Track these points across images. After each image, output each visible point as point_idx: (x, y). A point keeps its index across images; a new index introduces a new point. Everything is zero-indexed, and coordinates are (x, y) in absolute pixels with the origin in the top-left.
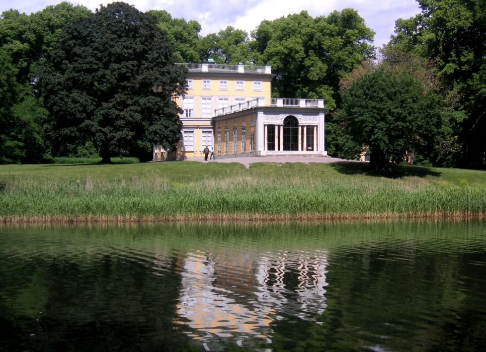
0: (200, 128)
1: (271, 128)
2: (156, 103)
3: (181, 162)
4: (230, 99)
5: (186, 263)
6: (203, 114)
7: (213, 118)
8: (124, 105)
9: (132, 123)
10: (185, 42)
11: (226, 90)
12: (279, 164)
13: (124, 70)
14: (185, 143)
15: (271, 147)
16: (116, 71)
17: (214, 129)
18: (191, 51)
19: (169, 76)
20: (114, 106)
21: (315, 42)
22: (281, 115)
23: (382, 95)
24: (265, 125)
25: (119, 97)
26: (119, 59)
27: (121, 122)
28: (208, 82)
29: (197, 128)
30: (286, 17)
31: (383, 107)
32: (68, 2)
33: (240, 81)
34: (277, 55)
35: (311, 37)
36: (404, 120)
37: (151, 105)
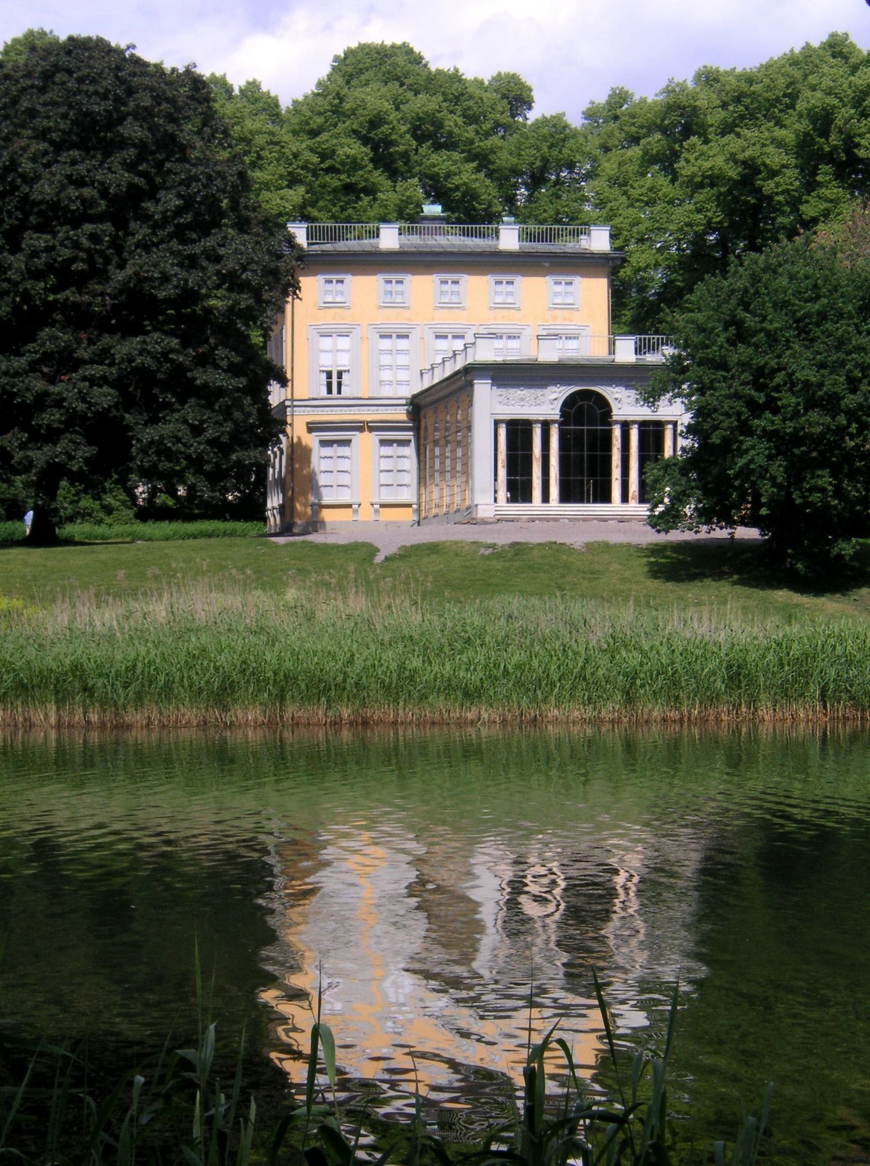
0: (372, 429)
1: (518, 433)
2: (165, 355)
3: (37, 555)
4: (415, 335)
5: (329, 853)
6: (382, 383)
7: (415, 397)
8: (65, 362)
9: (84, 417)
10: (451, 145)
11: (570, 307)
12: (488, 546)
13: (66, 253)
14: (322, 480)
15: (519, 490)
16: (38, 257)
17: (417, 430)
18: (467, 175)
19: (212, 268)
20: (33, 367)
21: (835, 139)
22: (554, 389)
23: (776, 322)
24: (497, 423)
25: (53, 337)
26: (52, 216)
27: (51, 417)
28: (398, 282)
29: (361, 429)
30: (181, 70)
31: (773, 363)
32: (47, 30)
33: (564, 279)
34: (712, 185)
35: (823, 121)
36: (831, 404)
37: (148, 361)
